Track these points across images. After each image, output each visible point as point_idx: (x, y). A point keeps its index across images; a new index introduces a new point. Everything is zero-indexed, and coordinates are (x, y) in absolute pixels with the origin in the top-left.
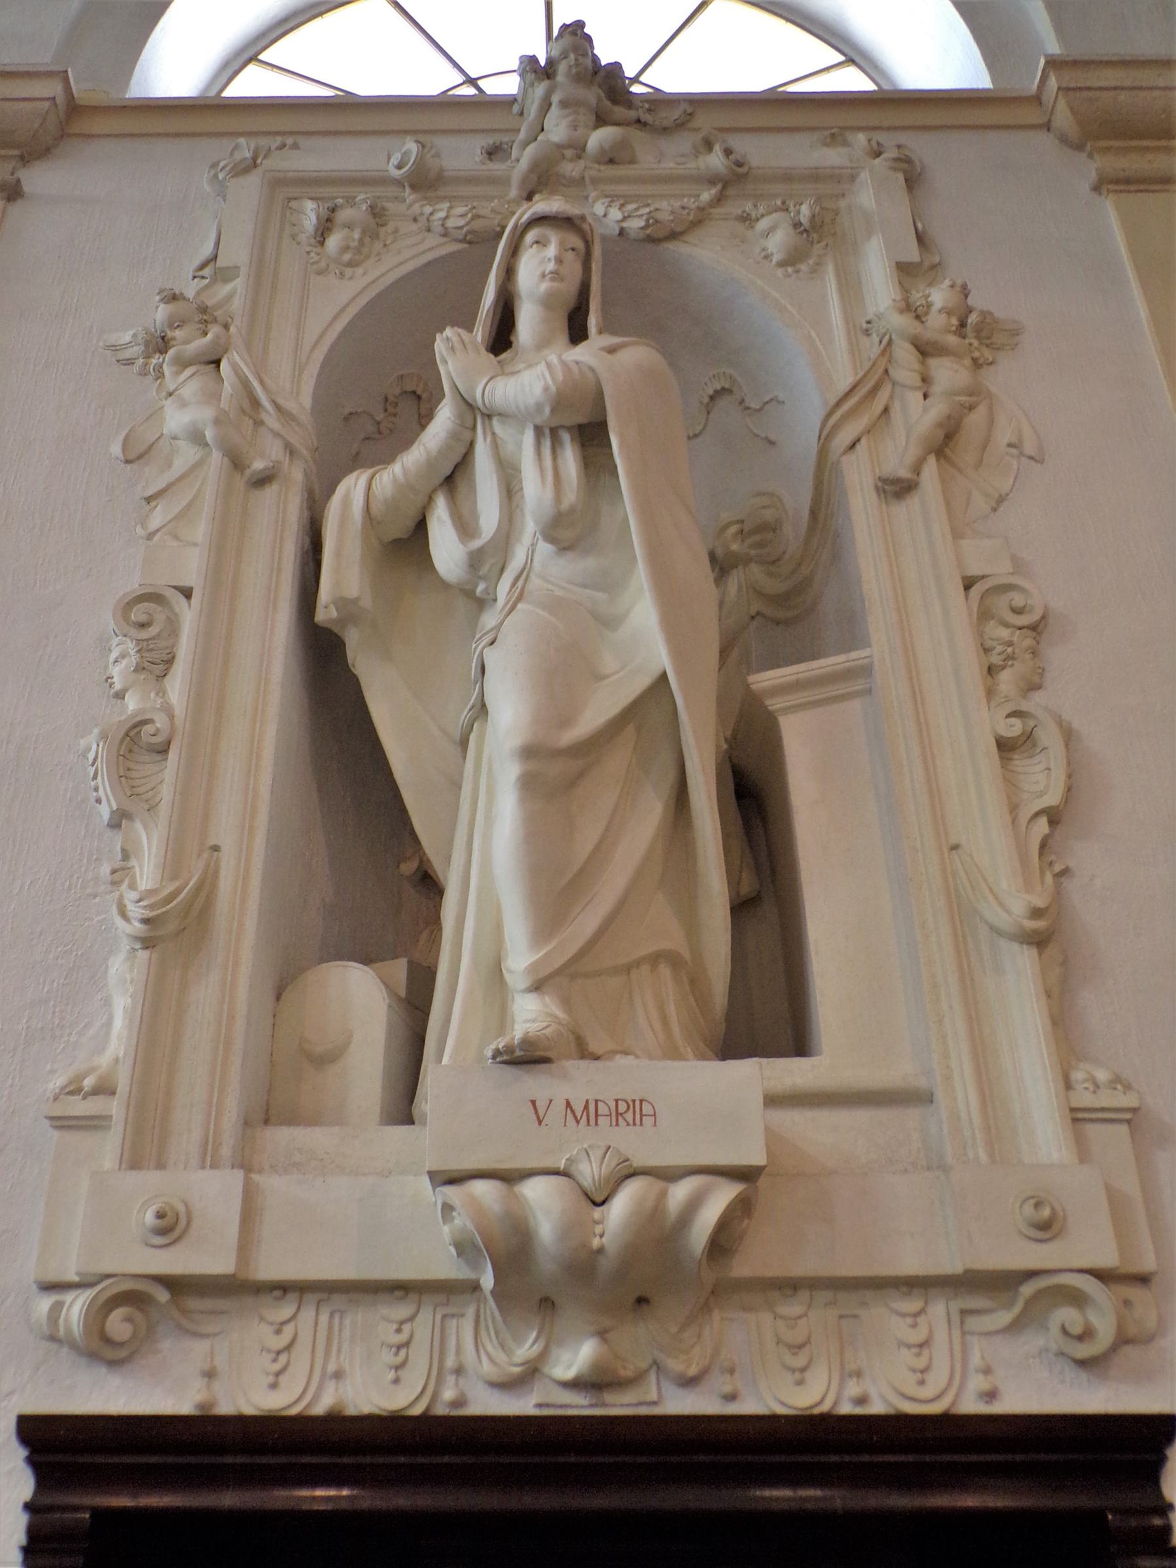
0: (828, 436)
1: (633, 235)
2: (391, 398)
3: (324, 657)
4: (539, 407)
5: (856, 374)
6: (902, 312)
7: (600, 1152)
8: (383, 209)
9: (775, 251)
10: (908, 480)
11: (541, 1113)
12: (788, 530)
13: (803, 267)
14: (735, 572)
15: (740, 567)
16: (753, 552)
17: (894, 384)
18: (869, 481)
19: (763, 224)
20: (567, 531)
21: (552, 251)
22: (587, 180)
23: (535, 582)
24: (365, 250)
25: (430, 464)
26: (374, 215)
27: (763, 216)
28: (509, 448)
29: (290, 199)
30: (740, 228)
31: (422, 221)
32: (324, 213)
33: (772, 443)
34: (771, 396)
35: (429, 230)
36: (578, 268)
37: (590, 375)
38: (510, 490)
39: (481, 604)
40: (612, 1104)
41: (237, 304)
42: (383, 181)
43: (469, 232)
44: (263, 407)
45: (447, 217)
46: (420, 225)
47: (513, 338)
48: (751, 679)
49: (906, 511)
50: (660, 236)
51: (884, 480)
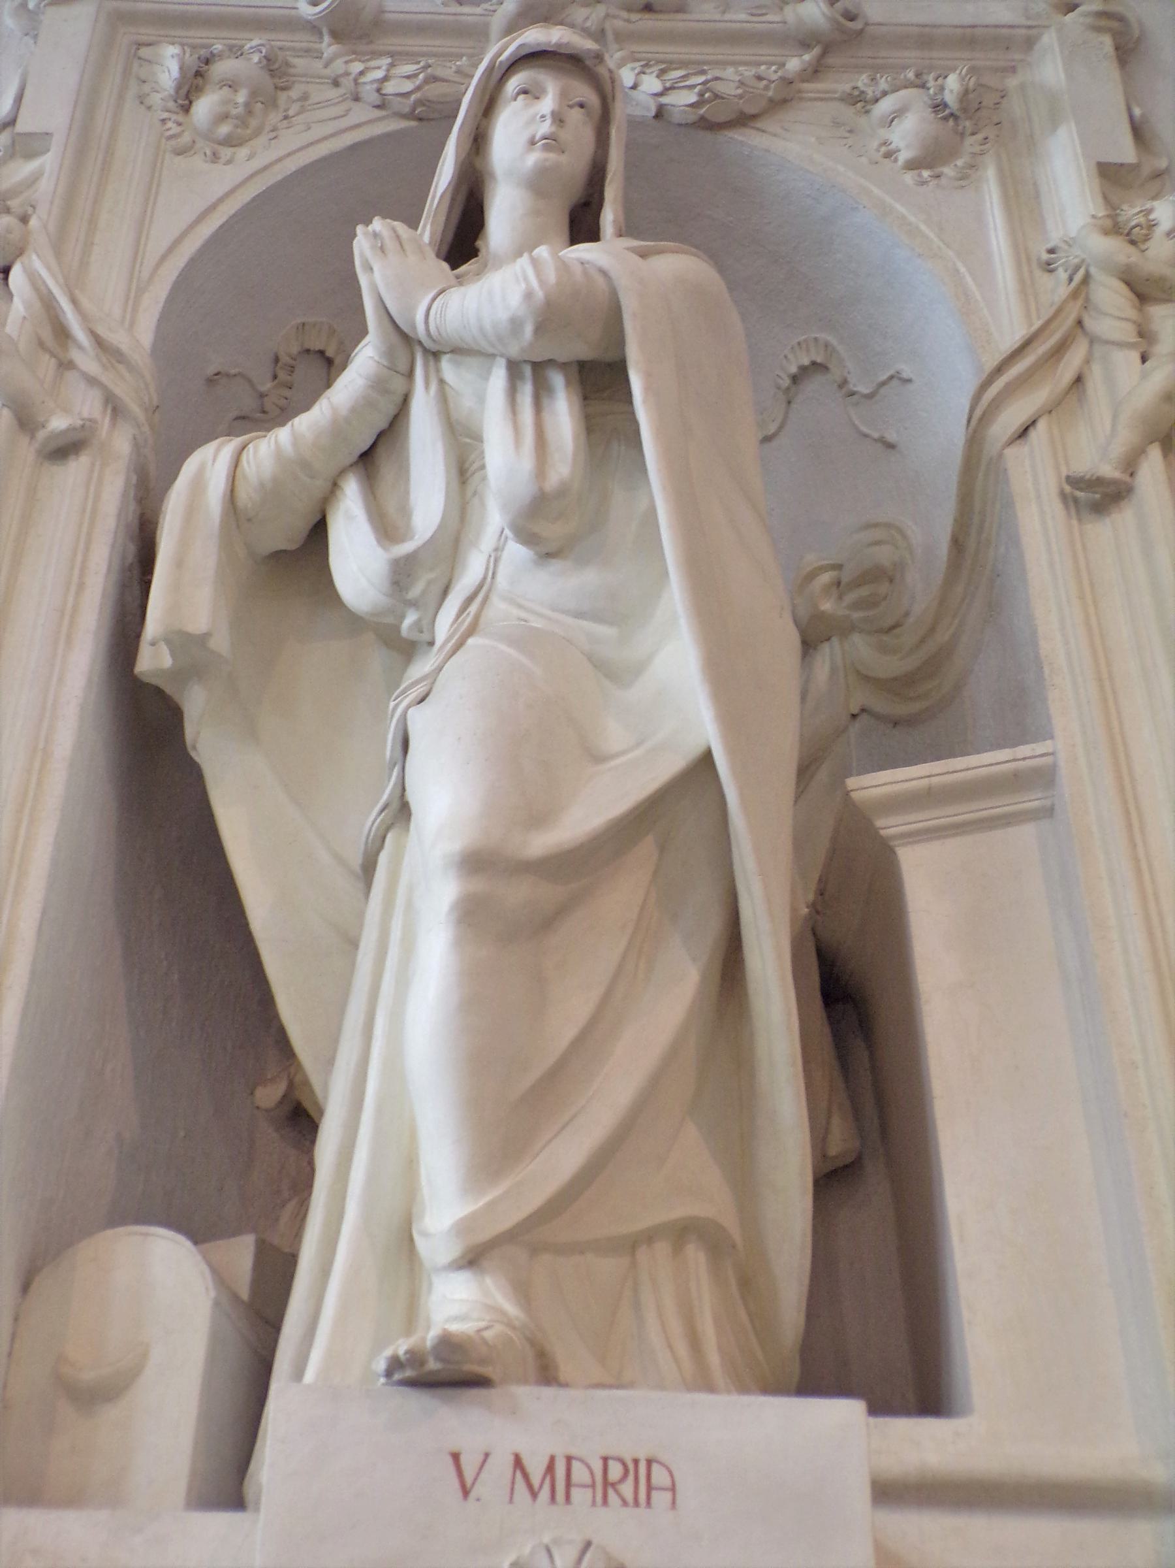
0: (981, 419)
1: (677, 117)
2: (284, 359)
3: (147, 736)
4: (515, 325)
5: (1031, 325)
6: (1106, 233)
7: (572, 1553)
8: (288, 64)
9: (902, 145)
10: (1114, 482)
11: (469, 1476)
12: (913, 577)
13: (948, 171)
14: (826, 648)
15: (835, 640)
16: (857, 615)
17: (1092, 341)
18: (1050, 485)
19: (886, 105)
20: (554, 526)
21: (547, 104)
22: (610, 36)
23: (498, 609)
24: (254, 123)
25: (338, 429)
26: (272, 73)
27: (885, 94)
28: (465, 402)
29: (140, 45)
30: (848, 113)
31: (347, 83)
32: (191, 60)
33: (891, 446)
34: (891, 372)
35: (357, 99)
36: (588, 136)
37: (600, 280)
38: (464, 468)
39: (407, 650)
40: (598, 1467)
41: (45, 186)
42: (292, 24)
43: (419, 102)
44: (75, 341)
45: (386, 79)
46: (341, 91)
47: (479, 243)
48: (852, 782)
49: (1109, 534)
50: (717, 121)
51: (1075, 482)
